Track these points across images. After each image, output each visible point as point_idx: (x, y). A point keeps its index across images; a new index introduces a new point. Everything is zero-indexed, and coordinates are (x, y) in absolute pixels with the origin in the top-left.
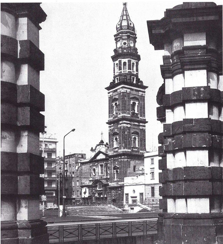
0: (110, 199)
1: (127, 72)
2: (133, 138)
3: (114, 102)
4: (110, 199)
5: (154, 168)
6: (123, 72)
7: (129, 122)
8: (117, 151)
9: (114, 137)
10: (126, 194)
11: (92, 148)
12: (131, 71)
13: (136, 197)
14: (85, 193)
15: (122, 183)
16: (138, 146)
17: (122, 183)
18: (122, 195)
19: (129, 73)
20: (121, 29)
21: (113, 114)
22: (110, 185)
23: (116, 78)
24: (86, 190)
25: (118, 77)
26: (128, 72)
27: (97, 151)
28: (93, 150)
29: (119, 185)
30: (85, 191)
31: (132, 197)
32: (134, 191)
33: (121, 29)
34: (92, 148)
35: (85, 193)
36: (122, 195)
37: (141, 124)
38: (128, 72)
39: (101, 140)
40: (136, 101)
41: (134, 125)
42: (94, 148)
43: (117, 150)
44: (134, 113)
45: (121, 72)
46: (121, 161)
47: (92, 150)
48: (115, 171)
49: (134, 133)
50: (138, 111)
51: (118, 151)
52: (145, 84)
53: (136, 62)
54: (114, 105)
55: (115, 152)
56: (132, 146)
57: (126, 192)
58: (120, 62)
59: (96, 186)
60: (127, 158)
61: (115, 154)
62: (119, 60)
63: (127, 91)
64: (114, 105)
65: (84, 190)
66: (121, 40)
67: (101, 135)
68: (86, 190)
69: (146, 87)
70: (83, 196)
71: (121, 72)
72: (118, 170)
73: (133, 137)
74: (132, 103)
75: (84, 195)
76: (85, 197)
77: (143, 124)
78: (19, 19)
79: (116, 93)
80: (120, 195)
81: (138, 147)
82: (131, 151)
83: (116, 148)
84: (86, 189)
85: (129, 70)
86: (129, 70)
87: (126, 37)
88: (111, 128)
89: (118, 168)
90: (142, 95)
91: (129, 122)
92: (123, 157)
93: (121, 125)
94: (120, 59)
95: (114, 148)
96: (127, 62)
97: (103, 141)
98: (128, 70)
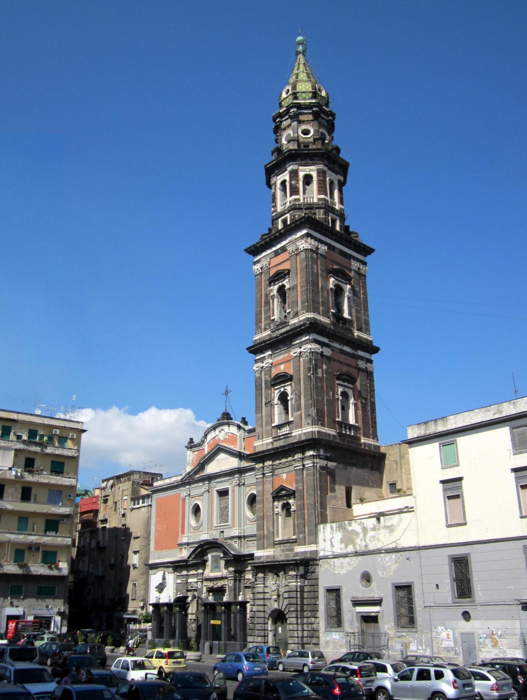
0: (261, 608)
1: (315, 201)
2: (339, 393)
3: (274, 285)
4: (261, 608)
5: (460, 479)
6: (302, 201)
7: (326, 340)
8: (286, 436)
9: (276, 392)
10: (329, 591)
11: (191, 439)
12: (328, 198)
13: (378, 602)
14: (161, 588)
15: (312, 548)
16: (357, 421)
17: (312, 548)
18: (311, 595)
19: (320, 202)
20: (296, 98)
21: (272, 318)
22: (260, 557)
23: (280, 220)
24: (164, 578)
25: (288, 215)
26: (319, 199)
27: (206, 449)
28: (196, 446)
29: (297, 554)
30: (161, 581)
31: (356, 603)
32: (367, 578)
33: (296, 98)
34: (191, 439)
35: (161, 588)
36: (311, 595)
37: (361, 353)
38: (319, 199)
39: (224, 411)
40: (344, 283)
41: (342, 352)
42: (196, 441)
43: (285, 430)
44: (338, 316)
45: (299, 200)
46: (303, 469)
47: (191, 445)
48: (279, 505)
49: (343, 377)
50: (350, 314)
51: (293, 434)
52: (364, 239)
53: (339, 181)
54: (275, 292)
55: (277, 438)
56: (337, 419)
57: (325, 582)
58: (294, 174)
59: (203, 564)
60: (327, 459)
61: (277, 444)
62: (289, 169)
63: (317, 248)
64: (275, 293)
65: (156, 578)
66: (295, 123)
67: (224, 396)
68: (164, 578)
69: (367, 251)
70: (154, 597)
71: (299, 200)
72: (291, 501)
73: (340, 390)
74: (331, 286)
75: (157, 594)
76: (161, 601)
77: (367, 355)
78: (60, 567)
79: (284, 256)
80: (302, 598)
81: (357, 424)
82: (335, 434)
83: (279, 427)
84: (166, 573)
85: (322, 196)
86: (322, 196)
87: (311, 117)
88: (265, 362)
89: (292, 494)
90: (359, 269)
91: (326, 340)
92: (311, 453)
93: (304, 347)
94: (295, 167)
95: (273, 425)
96: (314, 174)
97: (228, 414)
98: (319, 194)
